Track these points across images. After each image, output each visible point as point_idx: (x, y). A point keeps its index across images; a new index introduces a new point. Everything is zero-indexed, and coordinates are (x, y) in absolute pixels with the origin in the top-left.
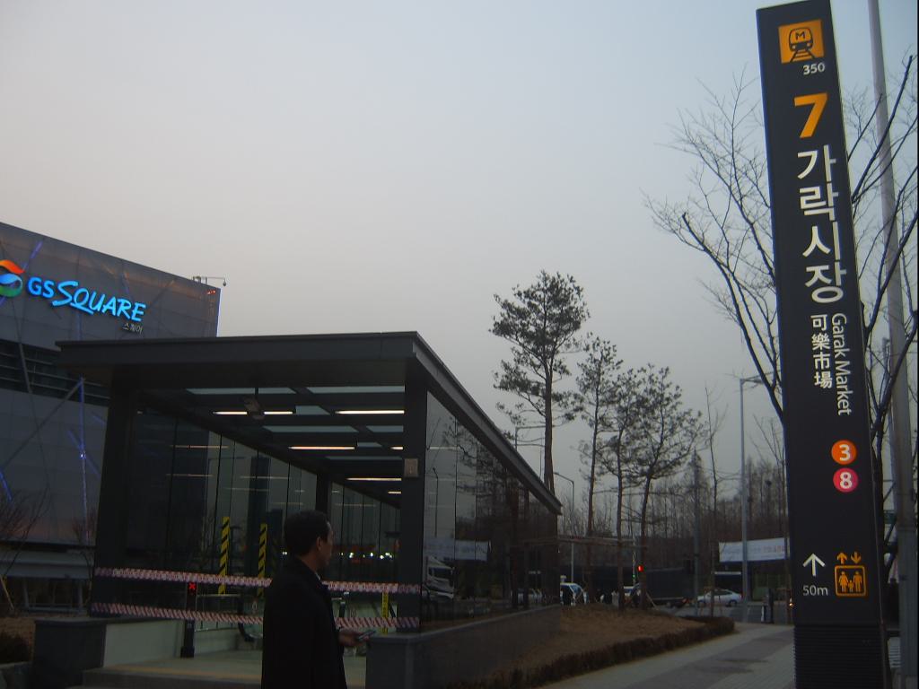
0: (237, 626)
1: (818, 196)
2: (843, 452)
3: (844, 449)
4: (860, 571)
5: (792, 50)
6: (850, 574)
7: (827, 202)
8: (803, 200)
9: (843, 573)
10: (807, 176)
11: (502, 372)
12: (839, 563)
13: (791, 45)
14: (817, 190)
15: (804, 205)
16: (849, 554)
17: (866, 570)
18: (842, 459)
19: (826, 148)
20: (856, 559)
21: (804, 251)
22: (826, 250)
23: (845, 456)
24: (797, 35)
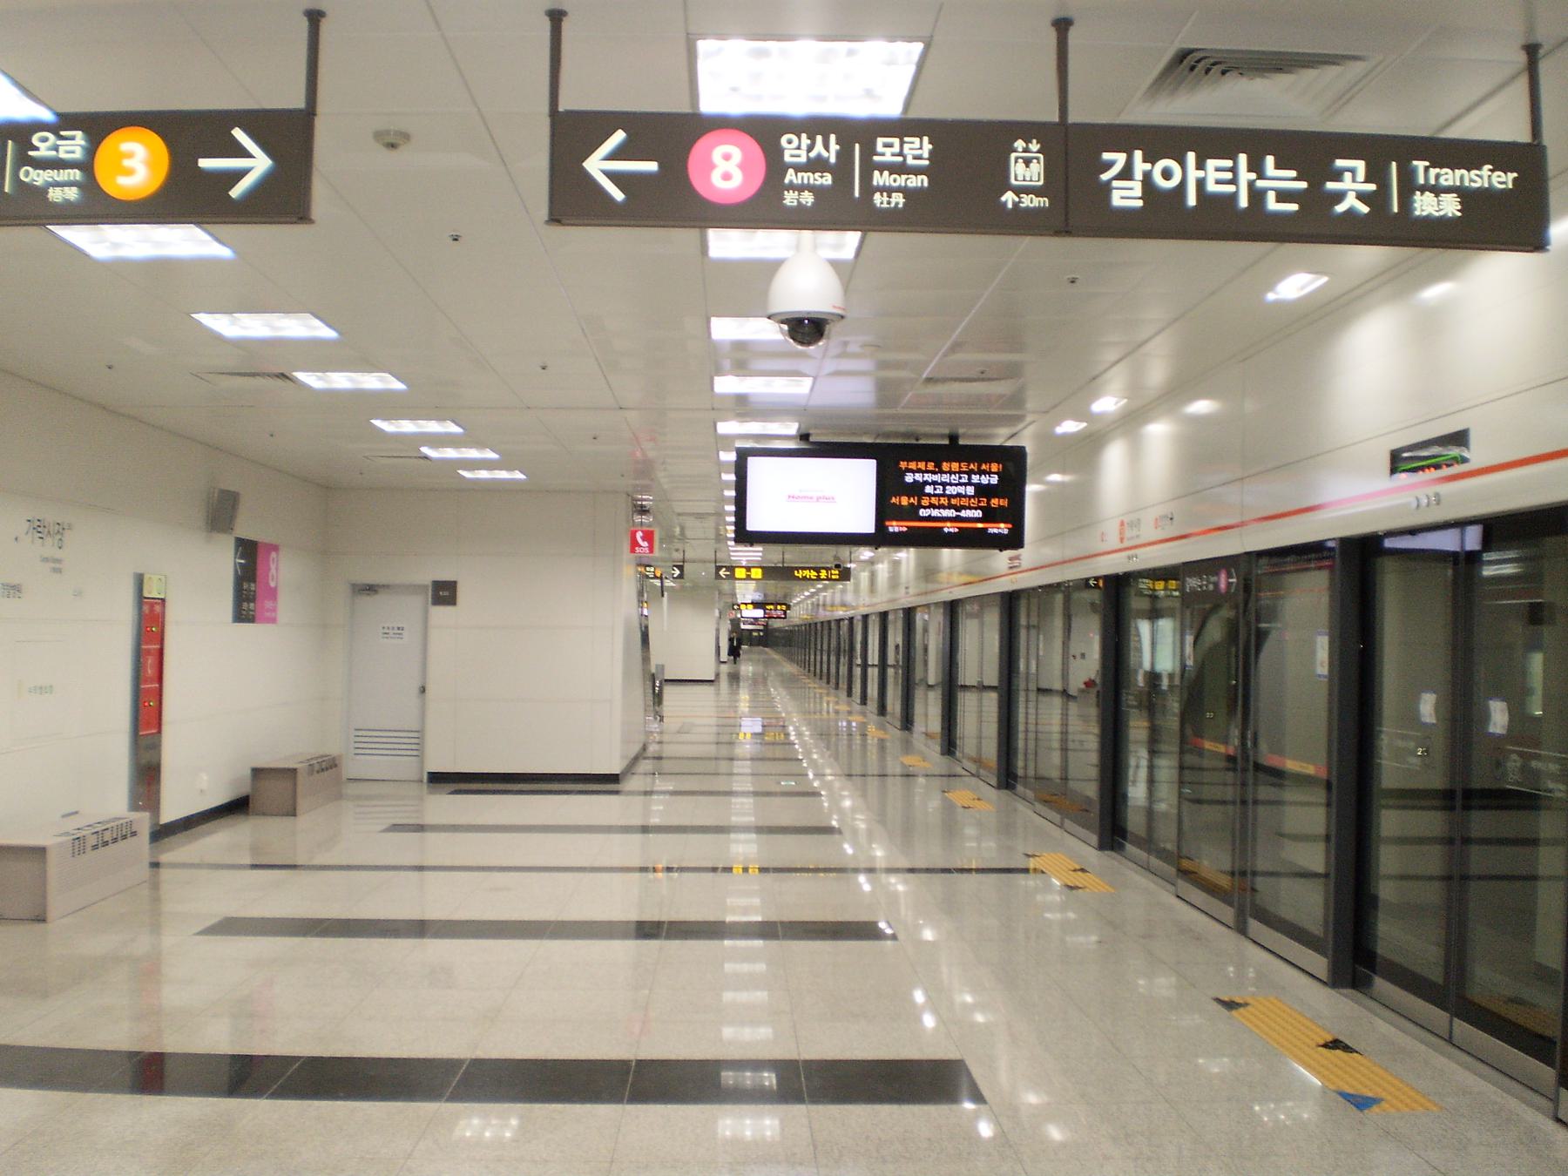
0: (1019, 779)
2: (127, 163)
3: (130, 155)
4: (1037, 159)
6: (1027, 162)
9: (1021, 160)
12: (1015, 151)
16: (1028, 141)
18: (123, 181)
20: (1034, 146)
21: (1102, 173)
23: (130, 172)
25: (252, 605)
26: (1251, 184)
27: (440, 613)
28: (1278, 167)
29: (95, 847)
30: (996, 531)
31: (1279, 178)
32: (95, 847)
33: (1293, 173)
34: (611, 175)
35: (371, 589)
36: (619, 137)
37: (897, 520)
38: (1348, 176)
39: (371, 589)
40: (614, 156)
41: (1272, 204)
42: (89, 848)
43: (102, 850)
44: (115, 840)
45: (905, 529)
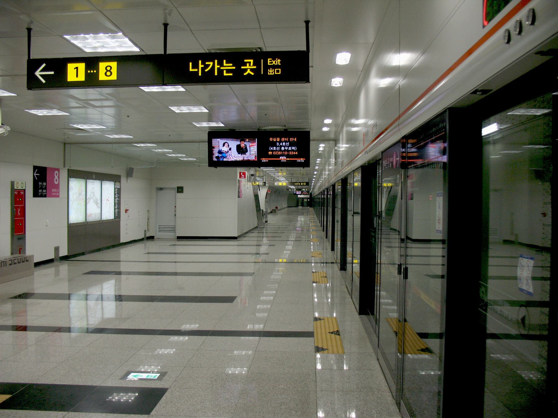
25: (44, 191)
26: (218, 69)
27: (179, 195)
28: (227, 63)
29: (10, 264)
30: (300, 161)
31: (227, 66)
32: (10, 264)
33: (231, 65)
34: (41, 75)
35: (161, 189)
36: (44, 65)
37: (265, 158)
38: (248, 64)
39: (161, 189)
40: (43, 70)
41: (225, 74)
42: (8, 265)
43: (13, 266)
44: (19, 263)
45: (267, 161)
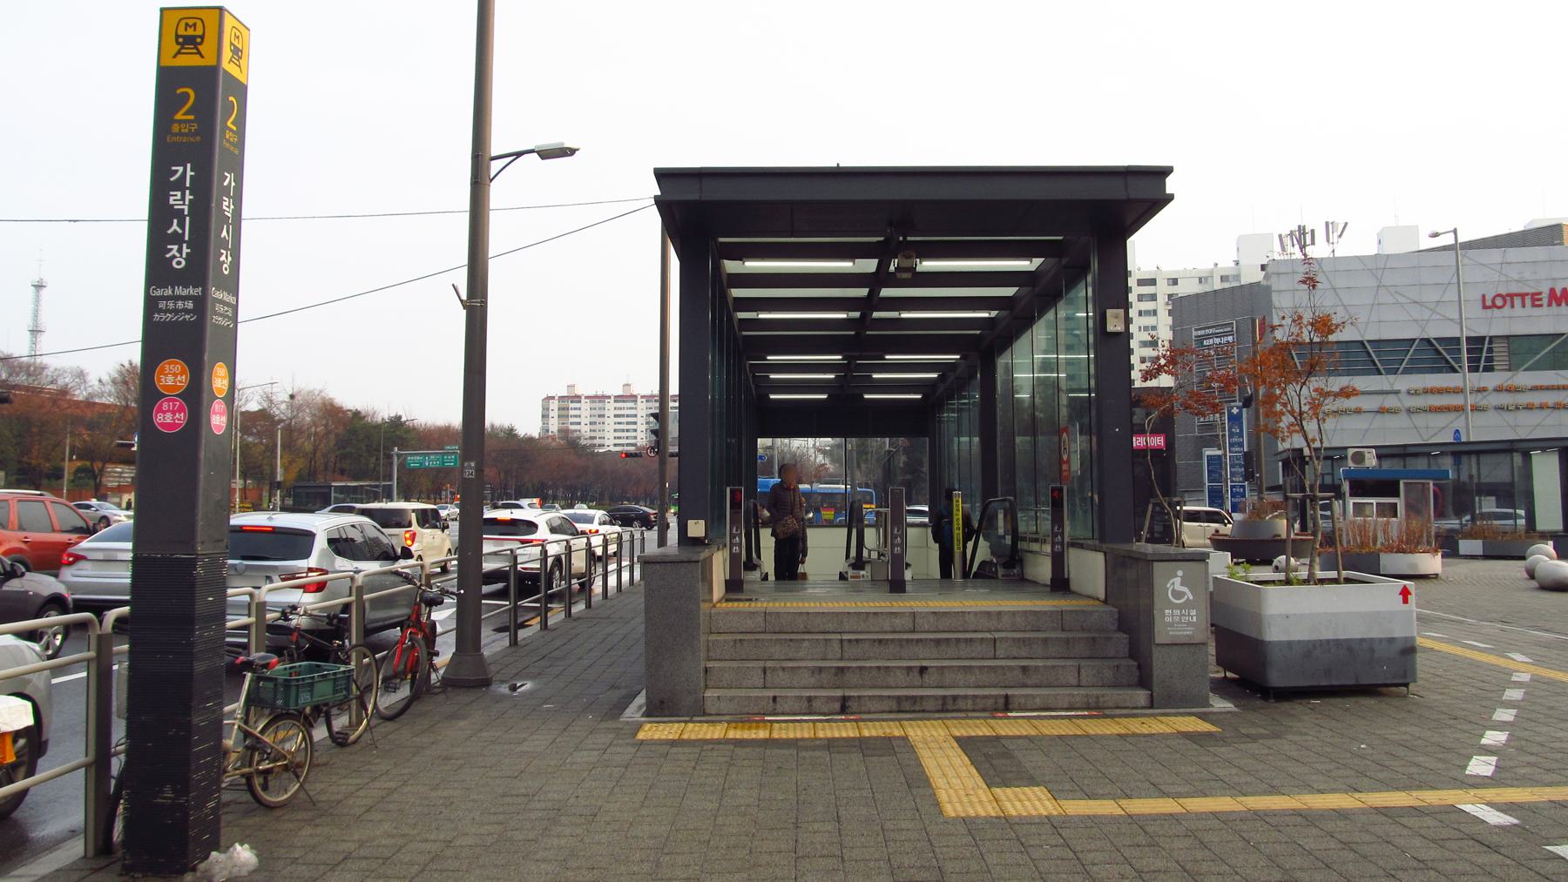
1: (179, 197)
5: (178, 43)
7: (184, 202)
8: (171, 198)
10: (177, 179)
11: (127, 365)
13: (177, 37)
14: (179, 194)
15: (171, 202)
17: (227, 121)
19: (189, 165)
22: (180, 231)
24: (187, 25)
